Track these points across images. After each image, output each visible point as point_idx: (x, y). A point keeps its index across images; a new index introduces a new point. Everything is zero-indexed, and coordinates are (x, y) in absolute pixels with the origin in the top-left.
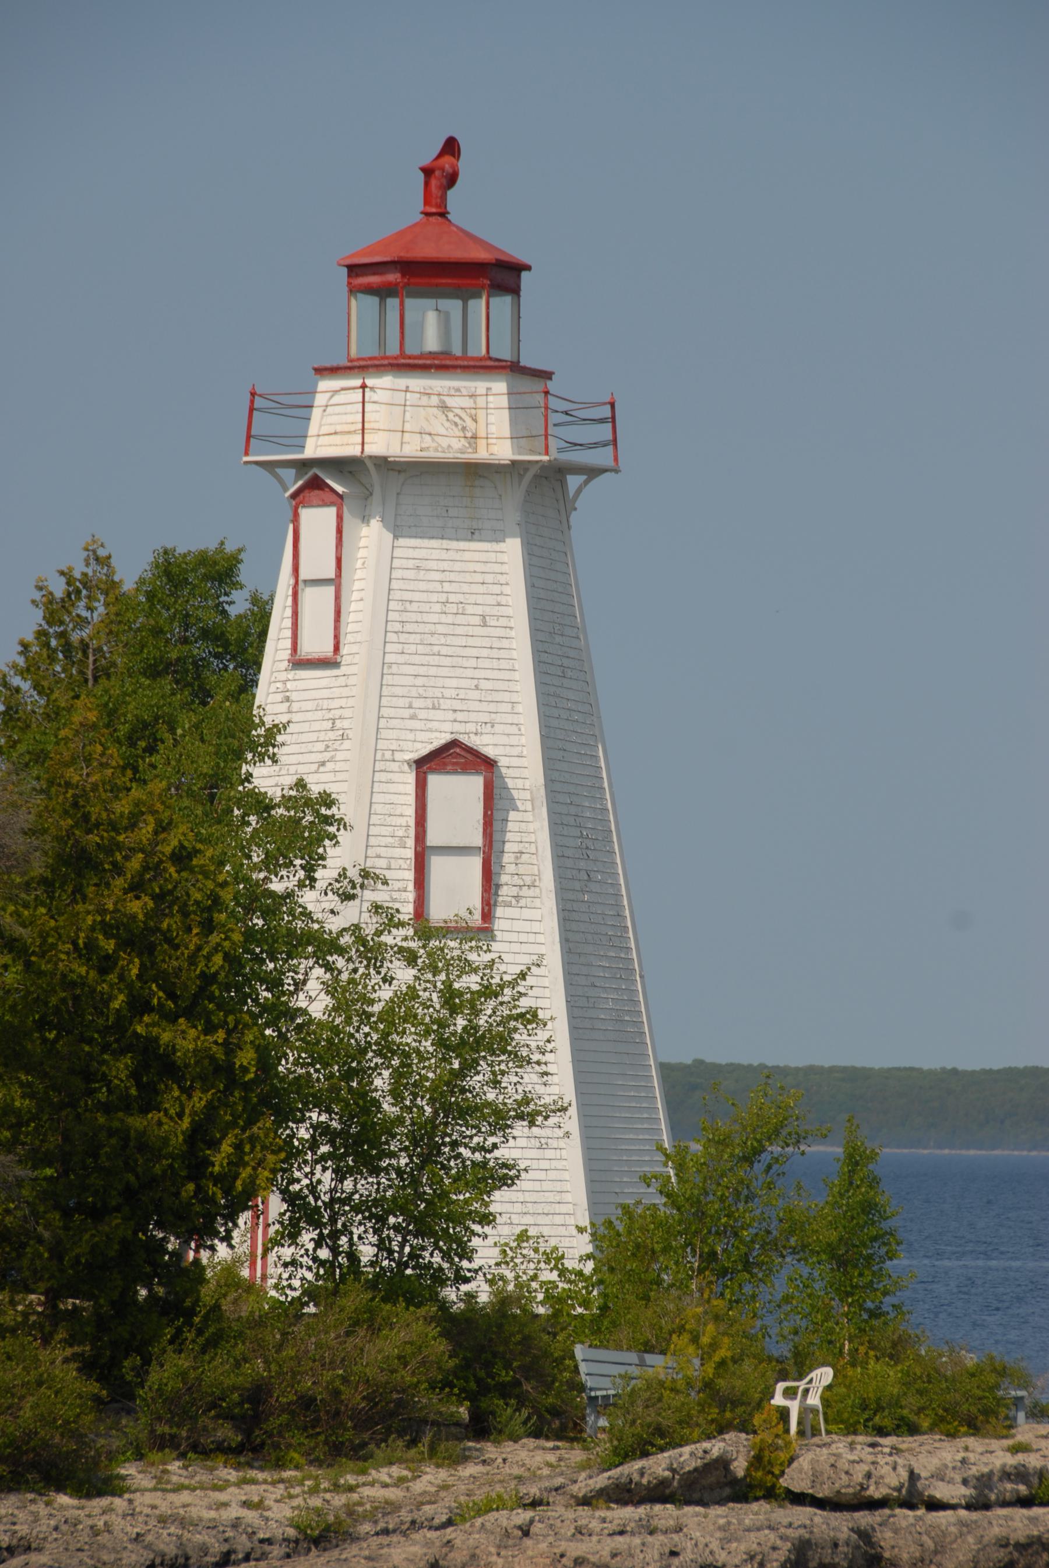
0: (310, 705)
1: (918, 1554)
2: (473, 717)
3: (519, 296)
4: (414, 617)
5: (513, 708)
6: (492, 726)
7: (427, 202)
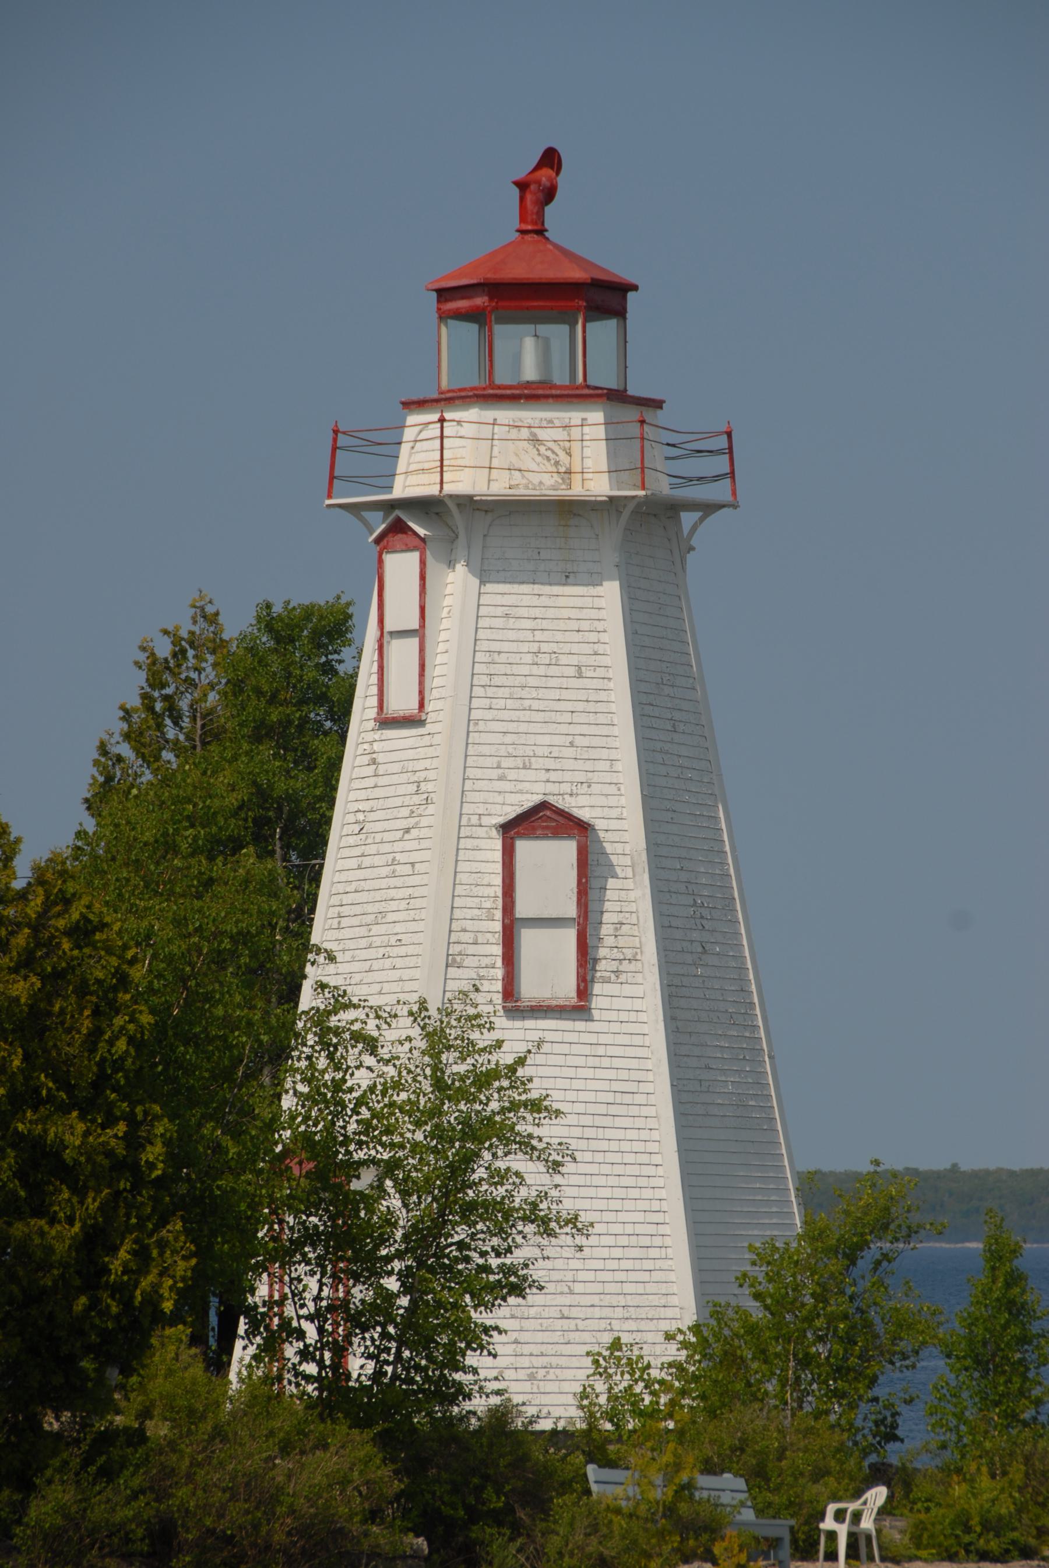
0: (396, 768)
2: (568, 776)
3: (625, 319)
4: (502, 669)
5: (612, 765)
6: (589, 787)
7: (523, 219)
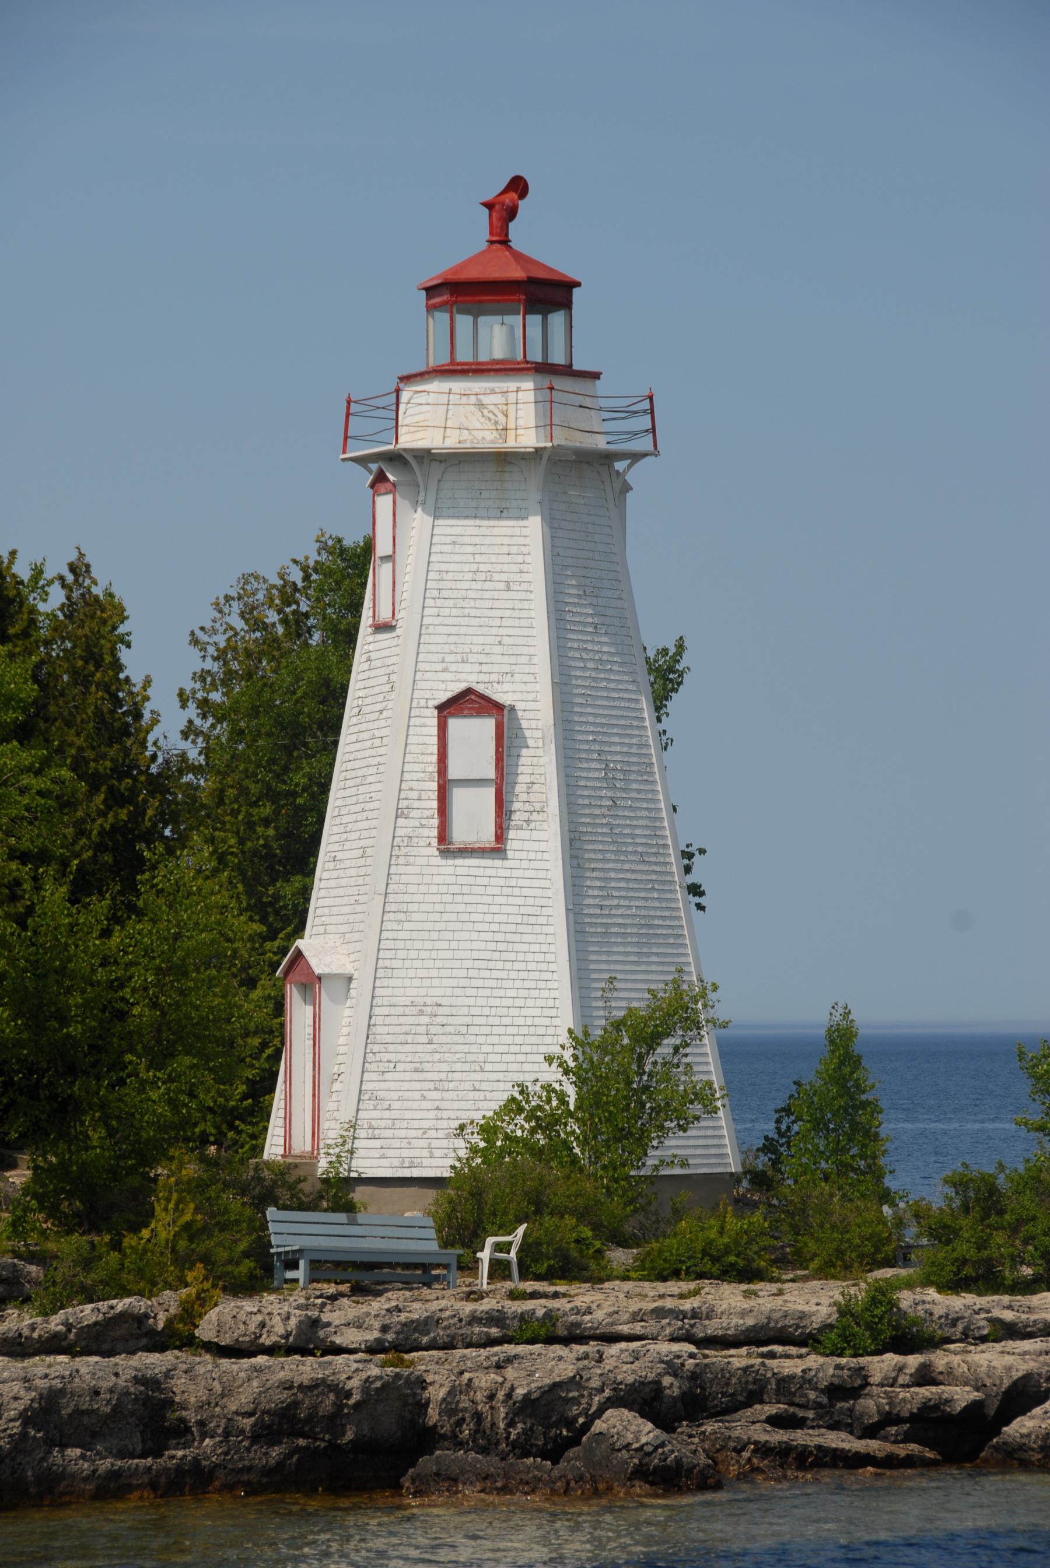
1: (204, 1398)
4: (449, 585)
7: (491, 233)
